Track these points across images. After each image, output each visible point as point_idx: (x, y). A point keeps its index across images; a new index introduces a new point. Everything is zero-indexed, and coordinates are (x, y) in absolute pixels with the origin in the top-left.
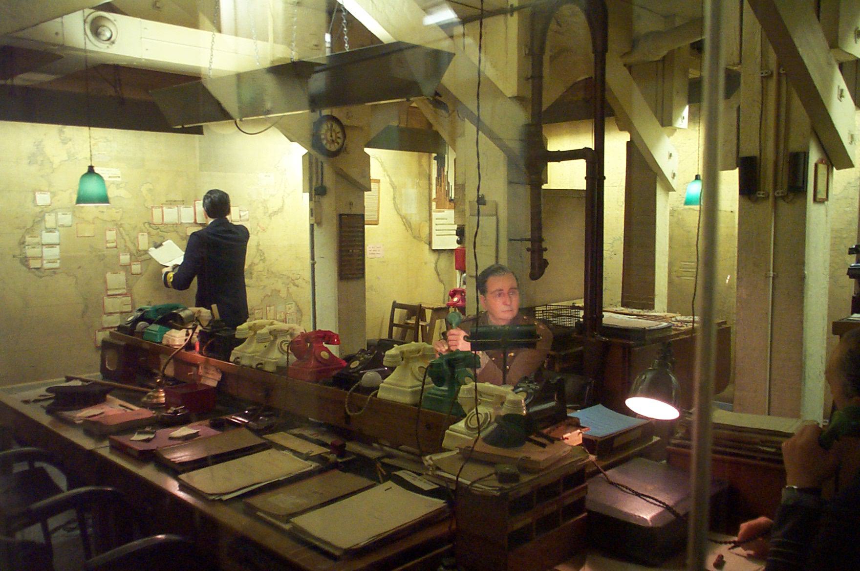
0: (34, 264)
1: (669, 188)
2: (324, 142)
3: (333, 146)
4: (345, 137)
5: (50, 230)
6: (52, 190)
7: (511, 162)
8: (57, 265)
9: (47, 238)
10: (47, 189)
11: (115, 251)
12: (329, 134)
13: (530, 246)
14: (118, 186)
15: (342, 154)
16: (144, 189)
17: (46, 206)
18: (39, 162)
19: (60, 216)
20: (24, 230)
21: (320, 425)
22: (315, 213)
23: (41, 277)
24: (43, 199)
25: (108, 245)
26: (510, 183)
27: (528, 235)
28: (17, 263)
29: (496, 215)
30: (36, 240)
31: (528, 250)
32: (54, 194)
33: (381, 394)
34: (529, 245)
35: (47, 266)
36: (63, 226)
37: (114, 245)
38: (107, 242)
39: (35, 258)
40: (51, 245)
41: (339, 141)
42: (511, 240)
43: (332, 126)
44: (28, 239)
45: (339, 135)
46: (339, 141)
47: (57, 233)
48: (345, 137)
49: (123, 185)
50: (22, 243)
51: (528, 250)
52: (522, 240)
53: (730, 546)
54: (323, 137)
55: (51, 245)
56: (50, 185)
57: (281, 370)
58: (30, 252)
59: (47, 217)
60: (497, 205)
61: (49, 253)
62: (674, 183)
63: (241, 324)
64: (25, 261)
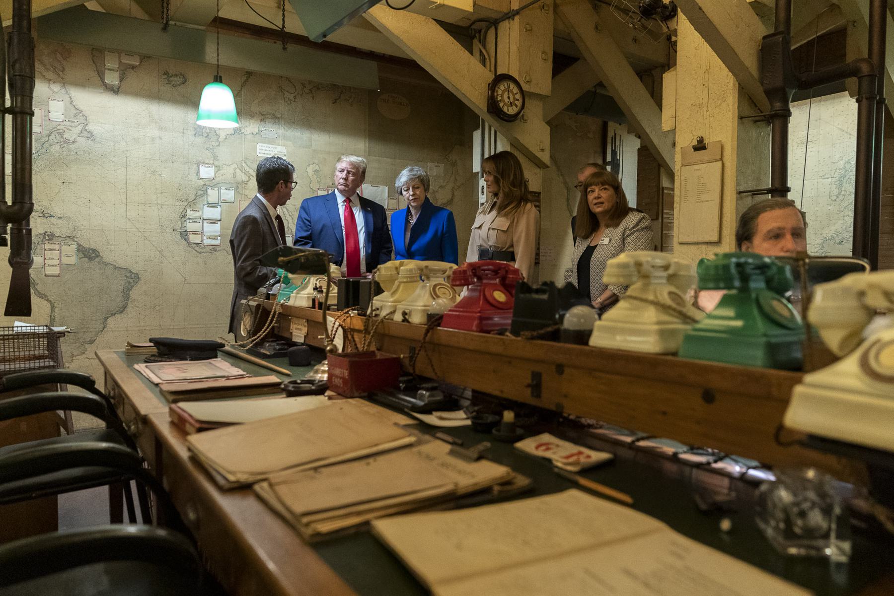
0: (193, 239)
2: (501, 105)
3: (510, 109)
5: (213, 205)
6: (217, 163)
7: (745, 94)
8: (217, 242)
9: (209, 213)
10: (211, 162)
17: (210, 180)
18: (205, 135)
19: (223, 191)
21: (520, 203)
23: (200, 253)
24: (207, 172)
26: (741, 118)
28: (177, 235)
29: (721, 159)
30: (198, 214)
32: (218, 168)
33: (597, 340)
35: (207, 242)
36: (225, 202)
39: (195, 233)
40: (213, 221)
41: (517, 102)
42: (740, 193)
43: (509, 87)
44: (189, 212)
45: (518, 96)
46: (517, 102)
47: (219, 209)
50: (184, 216)
53: (410, 422)
54: (499, 98)
55: (213, 221)
56: (215, 157)
57: (434, 320)
58: (190, 226)
59: (210, 191)
60: (722, 147)
61: (209, 228)
64: (185, 235)
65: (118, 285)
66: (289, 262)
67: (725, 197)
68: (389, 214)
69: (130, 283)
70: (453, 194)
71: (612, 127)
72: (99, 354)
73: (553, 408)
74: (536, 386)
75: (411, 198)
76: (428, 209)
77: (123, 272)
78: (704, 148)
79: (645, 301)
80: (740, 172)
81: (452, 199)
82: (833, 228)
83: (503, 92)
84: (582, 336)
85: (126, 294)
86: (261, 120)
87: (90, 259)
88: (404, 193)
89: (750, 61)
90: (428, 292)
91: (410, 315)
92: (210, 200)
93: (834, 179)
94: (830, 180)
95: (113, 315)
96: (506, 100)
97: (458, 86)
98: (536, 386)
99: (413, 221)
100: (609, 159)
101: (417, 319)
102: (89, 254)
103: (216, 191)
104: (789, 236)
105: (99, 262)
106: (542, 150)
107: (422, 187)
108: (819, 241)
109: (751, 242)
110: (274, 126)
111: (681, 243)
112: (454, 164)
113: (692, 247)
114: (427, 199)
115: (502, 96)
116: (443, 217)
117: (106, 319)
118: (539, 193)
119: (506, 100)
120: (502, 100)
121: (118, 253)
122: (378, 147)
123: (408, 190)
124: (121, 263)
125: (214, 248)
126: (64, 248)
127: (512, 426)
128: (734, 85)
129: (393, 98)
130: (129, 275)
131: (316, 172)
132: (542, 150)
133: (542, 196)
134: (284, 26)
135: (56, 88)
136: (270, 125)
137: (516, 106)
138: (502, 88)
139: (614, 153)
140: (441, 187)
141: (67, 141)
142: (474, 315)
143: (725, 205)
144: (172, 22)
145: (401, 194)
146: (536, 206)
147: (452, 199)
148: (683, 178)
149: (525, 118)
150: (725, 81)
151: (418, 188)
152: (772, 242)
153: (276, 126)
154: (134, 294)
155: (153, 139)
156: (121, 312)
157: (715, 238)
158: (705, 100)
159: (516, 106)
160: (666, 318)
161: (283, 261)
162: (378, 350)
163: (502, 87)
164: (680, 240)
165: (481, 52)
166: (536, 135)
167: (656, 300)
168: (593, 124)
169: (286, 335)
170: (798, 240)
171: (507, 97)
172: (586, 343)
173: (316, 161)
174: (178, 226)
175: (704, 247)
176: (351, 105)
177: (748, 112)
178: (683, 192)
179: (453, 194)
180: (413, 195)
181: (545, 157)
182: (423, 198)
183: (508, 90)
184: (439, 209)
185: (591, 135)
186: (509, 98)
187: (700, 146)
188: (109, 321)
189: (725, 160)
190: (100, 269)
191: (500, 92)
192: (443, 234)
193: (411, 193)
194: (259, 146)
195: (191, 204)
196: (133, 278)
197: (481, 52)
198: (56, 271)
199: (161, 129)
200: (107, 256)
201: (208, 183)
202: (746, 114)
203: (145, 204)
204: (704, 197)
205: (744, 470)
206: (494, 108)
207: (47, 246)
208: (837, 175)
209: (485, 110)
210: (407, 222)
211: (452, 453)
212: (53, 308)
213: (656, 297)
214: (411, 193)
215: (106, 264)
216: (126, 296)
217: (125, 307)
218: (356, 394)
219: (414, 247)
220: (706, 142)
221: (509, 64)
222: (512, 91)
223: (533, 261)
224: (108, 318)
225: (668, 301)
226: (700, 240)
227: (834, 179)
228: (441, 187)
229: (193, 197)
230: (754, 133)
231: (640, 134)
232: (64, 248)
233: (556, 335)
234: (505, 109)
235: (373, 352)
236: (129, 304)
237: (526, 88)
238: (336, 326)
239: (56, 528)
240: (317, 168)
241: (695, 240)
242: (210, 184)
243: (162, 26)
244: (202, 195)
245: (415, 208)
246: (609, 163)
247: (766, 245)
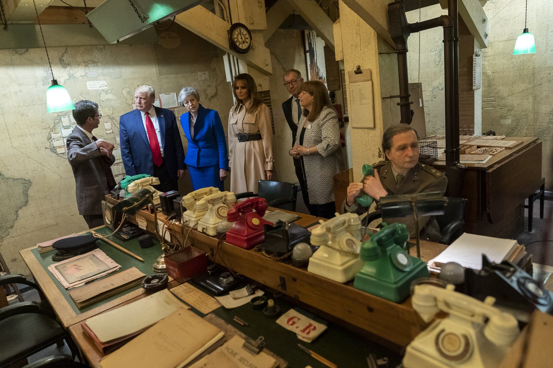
1: (483, 46)
2: (238, 44)
3: (244, 45)
4: (251, 39)
7: (381, 38)
11: (112, 136)
12: (239, 37)
13: (399, 102)
14: (106, 92)
15: (251, 51)
16: (124, 92)
20: (49, 130)
22: (76, 181)
25: (108, 132)
26: (380, 54)
27: (397, 92)
28: (48, 151)
29: (371, 80)
31: (398, 104)
33: (311, 269)
34: (398, 100)
37: (111, 131)
38: (106, 130)
41: (247, 40)
43: (240, 31)
44: (53, 135)
45: (247, 36)
46: (247, 40)
48: (251, 39)
49: (110, 91)
50: (50, 138)
51: (398, 104)
52: (391, 97)
54: (236, 40)
57: (221, 235)
59: (63, 119)
60: (371, 72)
62: (486, 41)
63: (186, 194)
65: (18, 190)
66: (129, 210)
67: (375, 102)
68: (178, 115)
69: (26, 187)
70: (217, 89)
71: (306, 32)
73: (293, 296)
74: (283, 284)
75: (191, 107)
76: (202, 112)
77: (20, 181)
78: (361, 73)
79: (334, 249)
80: (382, 85)
81: (216, 93)
82: (438, 81)
83: (238, 36)
84: (305, 264)
85: (26, 194)
86: (85, 66)
88: (186, 105)
89: (382, 21)
90: (214, 214)
91: (207, 230)
92: (64, 125)
93: (437, 52)
94: (434, 52)
95: (20, 208)
96: (240, 40)
97: (209, 37)
98: (283, 284)
99: (194, 120)
100: (307, 49)
101: (211, 232)
103: (67, 118)
104: (409, 148)
105: (2, 179)
106: (267, 65)
107: (196, 99)
108: (431, 89)
109: (390, 151)
110: (95, 68)
111: (354, 128)
112: (214, 70)
113: (360, 130)
114: (200, 105)
115: (237, 38)
116: (212, 114)
117: (17, 212)
118: (269, 91)
119: (240, 40)
122: (165, 69)
123: (187, 102)
124: (17, 176)
127: (274, 308)
128: (374, 34)
129: (170, 45)
130: (24, 182)
132: (267, 65)
133: (270, 92)
134: (85, 4)
136: (92, 68)
137: (247, 42)
138: (236, 33)
139: (310, 44)
140: (209, 86)
142: (243, 238)
143: (376, 106)
144: (8, 23)
145: (184, 106)
146: (268, 106)
147: (216, 93)
148: (351, 90)
149: (254, 47)
150: (369, 33)
151: (193, 100)
152: (401, 152)
153: (96, 68)
154: (31, 192)
155: (16, 93)
156: (26, 205)
157: (372, 125)
158: (359, 43)
159: (247, 42)
160: (346, 259)
161: (126, 210)
162: (192, 245)
163: (236, 32)
164: (353, 126)
165: (219, 5)
166: (262, 56)
167: (340, 249)
168: (296, 32)
169: (134, 223)
170: (415, 149)
171: (240, 37)
172: (306, 270)
173: (127, 86)
174: (48, 145)
175: (366, 130)
177: (384, 49)
178: (352, 98)
179: (217, 89)
180: (192, 106)
181: (269, 69)
182: (198, 106)
183: (240, 33)
184: (209, 111)
185: (295, 35)
186: (242, 38)
187: (359, 71)
188: (19, 212)
189: (373, 80)
190: (4, 182)
191: (235, 36)
192: (213, 127)
193: (190, 104)
194: (88, 83)
195: (53, 129)
196: (27, 184)
197: (219, 5)
199: (20, 85)
201: (60, 114)
202: (384, 51)
203: (22, 136)
204: (364, 101)
206: (233, 46)
208: (438, 49)
209: (228, 48)
210: (190, 122)
211: (244, 346)
213: (340, 246)
214: (190, 104)
215: (8, 179)
217: (27, 202)
218: (185, 280)
219: (197, 138)
220: (362, 69)
221: (239, 16)
222: (243, 34)
223: (272, 132)
224: (18, 211)
225: (346, 248)
226: (364, 126)
227: (437, 52)
228: (209, 86)
229: (53, 125)
230: (387, 58)
231: (324, 38)
233: (289, 260)
234: (240, 47)
235: (189, 247)
236: (29, 199)
237: (250, 27)
238: (164, 230)
240: (129, 90)
241: (361, 126)
243: (3, 26)
244: (58, 123)
245: (194, 113)
246: (308, 51)
247: (398, 153)
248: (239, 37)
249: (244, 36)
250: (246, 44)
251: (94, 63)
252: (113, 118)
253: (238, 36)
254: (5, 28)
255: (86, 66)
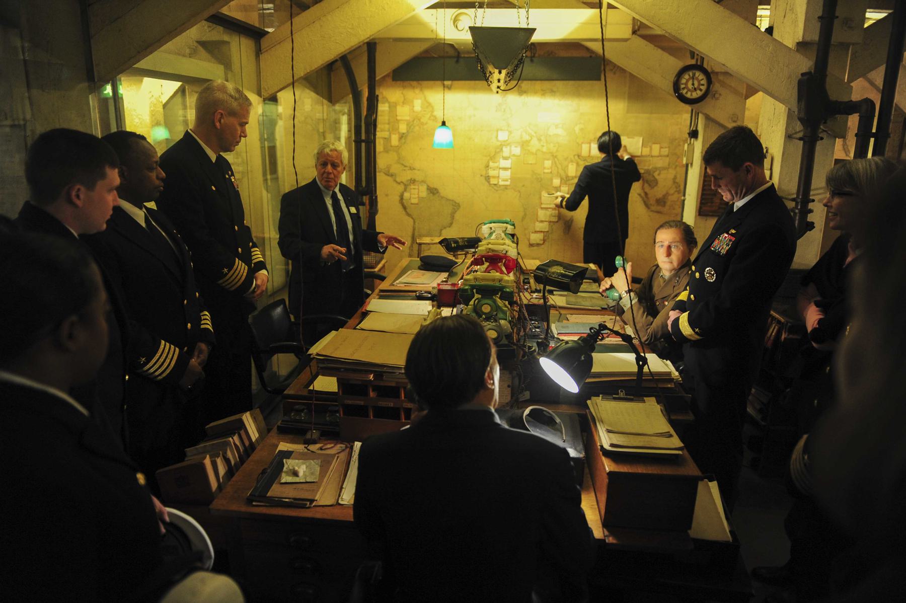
0: (493, 181)
5: (505, 158)
8: (508, 183)
9: (504, 163)
12: (690, 82)
15: (708, 99)
16: (577, 129)
24: (503, 136)
25: (546, 171)
28: (483, 179)
30: (496, 165)
32: (510, 132)
35: (501, 183)
38: (544, 168)
39: (494, 177)
40: (505, 169)
41: (702, 87)
44: (491, 164)
45: (704, 82)
46: (702, 87)
50: (487, 166)
55: (505, 169)
56: (508, 125)
58: (492, 173)
59: (504, 149)
64: (488, 178)
72: (712, 115)
83: (687, 81)
87: (434, 194)
96: (690, 86)
102: (433, 191)
115: (686, 84)
120: (686, 87)
121: (449, 191)
124: (450, 197)
125: (506, 187)
126: (421, 187)
131: (581, 130)
135: (417, 91)
137: (701, 90)
141: (423, 124)
154: (457, 216)
156: (433, 108)
159: (701, 90)
174: (484, 173)
176: (615, 73)
186: (693, 84)
191: (684, 81)
196: (456, 206)
198: (415, 201)
200: (443, 192)
205: (633, 336)
207: (412, 187)
212: (414, 222)
215: (442, 197)
216: (453, 217)
217: (451, 224)
222: (697, 79)
232: (421, 187)
239: (256, 308)
242: (505, 144)
248: (690, 82)
249: (699, 82)
250: (698, 92)
251: (552, 92)
252: (556, 157)
253: (687, 81)
254: (457, 61)
255: (543, 95)
